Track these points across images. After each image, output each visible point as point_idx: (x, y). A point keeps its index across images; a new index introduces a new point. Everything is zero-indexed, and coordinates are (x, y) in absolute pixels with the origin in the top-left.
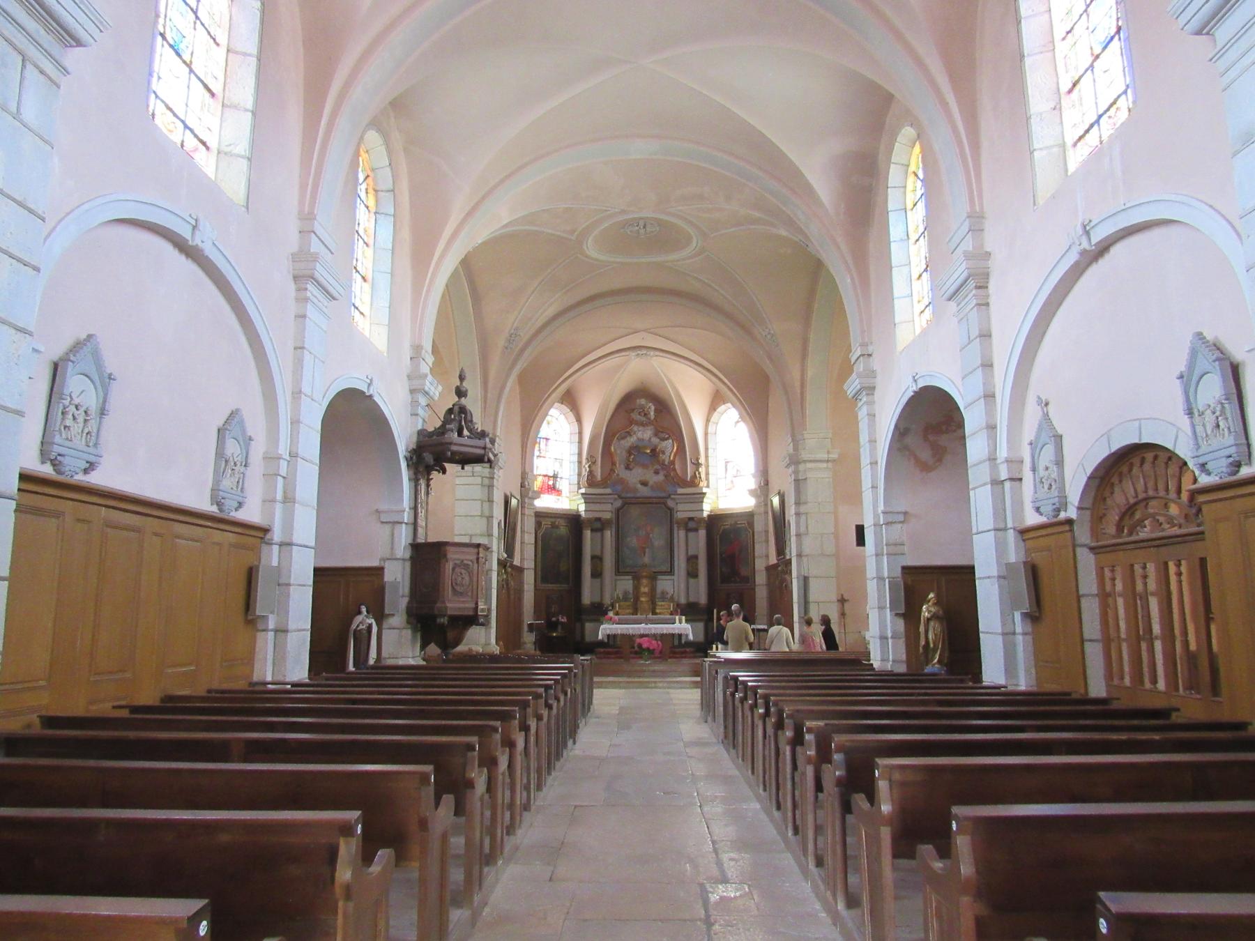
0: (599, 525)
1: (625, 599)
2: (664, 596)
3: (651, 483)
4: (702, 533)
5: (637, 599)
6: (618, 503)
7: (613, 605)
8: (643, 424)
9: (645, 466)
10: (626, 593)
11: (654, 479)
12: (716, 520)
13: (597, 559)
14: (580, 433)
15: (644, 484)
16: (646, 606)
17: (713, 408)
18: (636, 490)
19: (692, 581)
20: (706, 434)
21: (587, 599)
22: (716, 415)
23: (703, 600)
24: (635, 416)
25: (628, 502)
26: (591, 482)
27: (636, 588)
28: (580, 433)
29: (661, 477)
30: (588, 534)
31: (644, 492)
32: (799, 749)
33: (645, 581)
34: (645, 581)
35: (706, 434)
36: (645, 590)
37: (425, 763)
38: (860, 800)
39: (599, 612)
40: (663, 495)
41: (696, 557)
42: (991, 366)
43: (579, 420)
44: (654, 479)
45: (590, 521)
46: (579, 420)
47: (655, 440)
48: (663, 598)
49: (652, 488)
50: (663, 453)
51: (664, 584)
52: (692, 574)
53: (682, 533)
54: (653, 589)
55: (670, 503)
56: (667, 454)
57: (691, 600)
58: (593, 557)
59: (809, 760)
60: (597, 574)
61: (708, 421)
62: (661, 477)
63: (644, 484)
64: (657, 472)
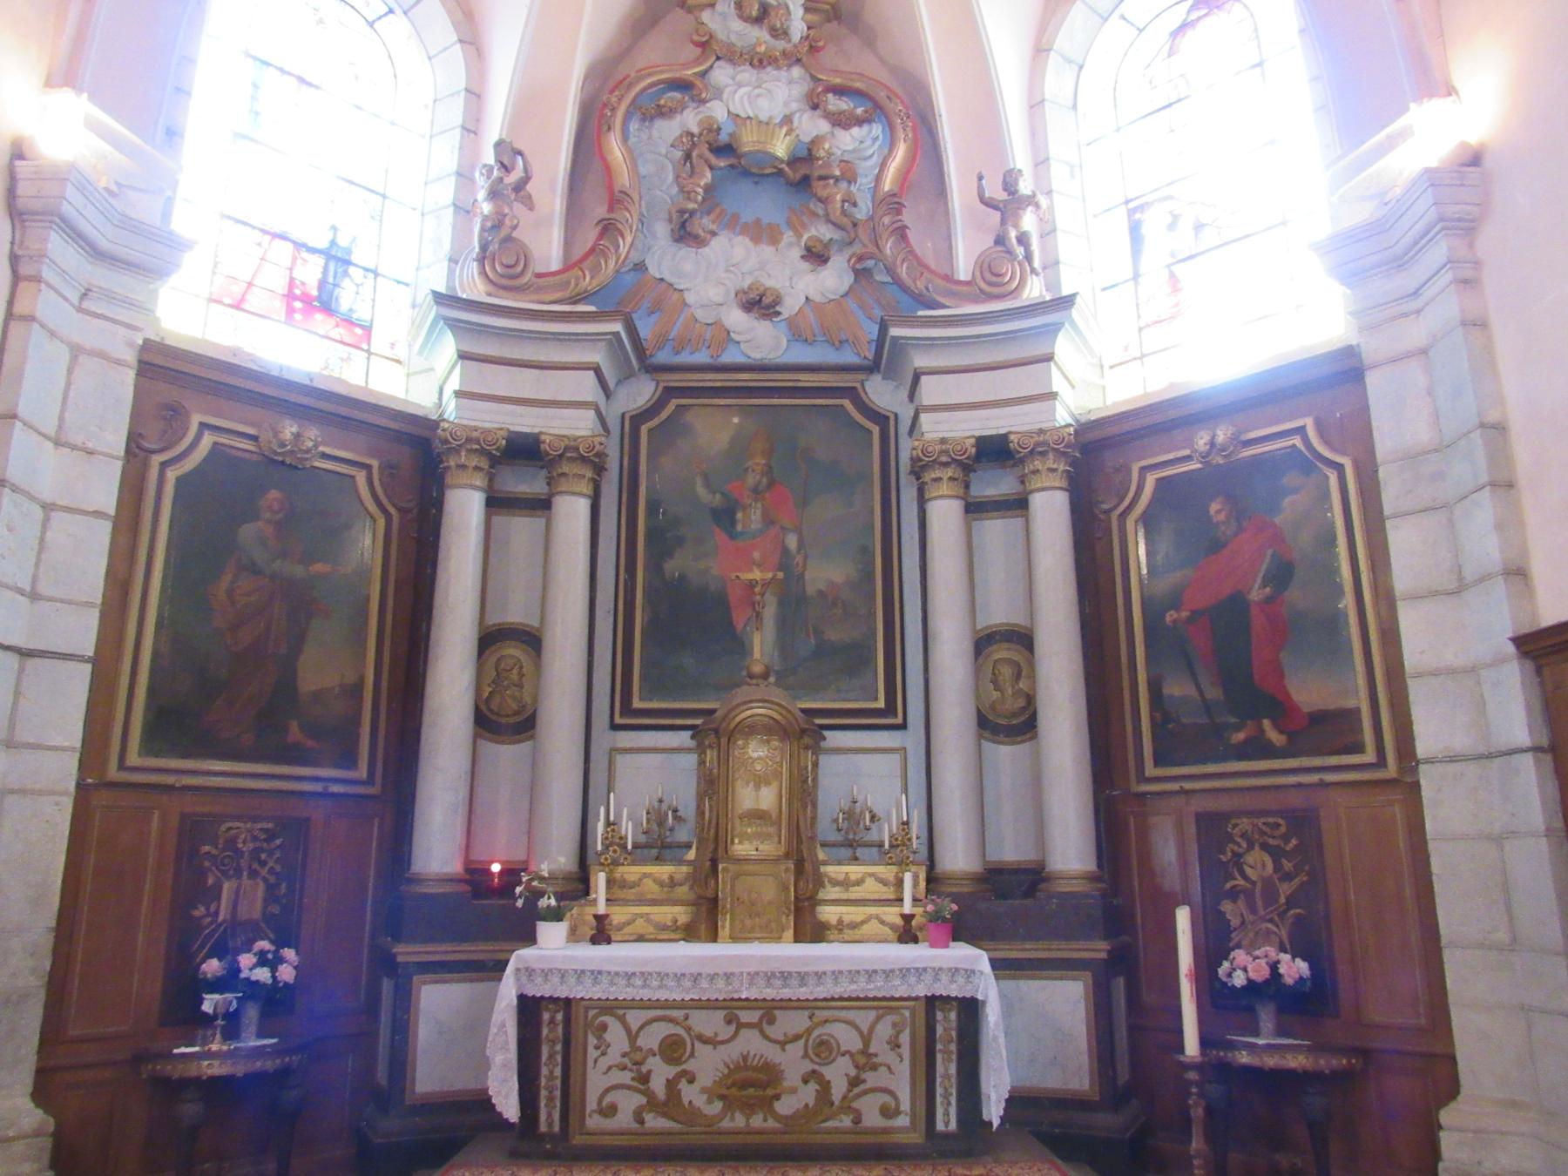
1: (657, 845)
3: (791, 305)
4: (1051, 509)
5: (732, 903)
7: (578, 885)
8: (760, 61)
9: (761, 233)
10: (659, 816)
11: (807, 286)
12: (1095, 458)
13: (507, 644)
14: (475, 95)
15: (760, 304)
16: (768, 888)
18: (725, 337)
19: (1004, 754)
20: (1035, 105)
21: (437, 850)
23: (1071, 851)
25: (678, 387)
26: (501, 253)
27: (713, 786)
28: (475, 95)
29: (833, 279)
30: (465, 508)
31: (761, 341)
35: (1035, 105)
36: (757, 796)
37: (959, 1121)
40: (848, 357)
41: (1023, 639)
42: (1510, 485)
44: (807, 286)
45: (476, 443)
47: (811, 126)
48: (852, 844)
49: (798, 334)
50: (850, 176)
51: (864, 773)
52: (1009, 722)
53: (945, 513)
54: (803, 792)
55: (882, 393)
58: (489, 639)
60: (504, 719)
62: (833, 279)
63: (760, 304)
64: (816, 256)
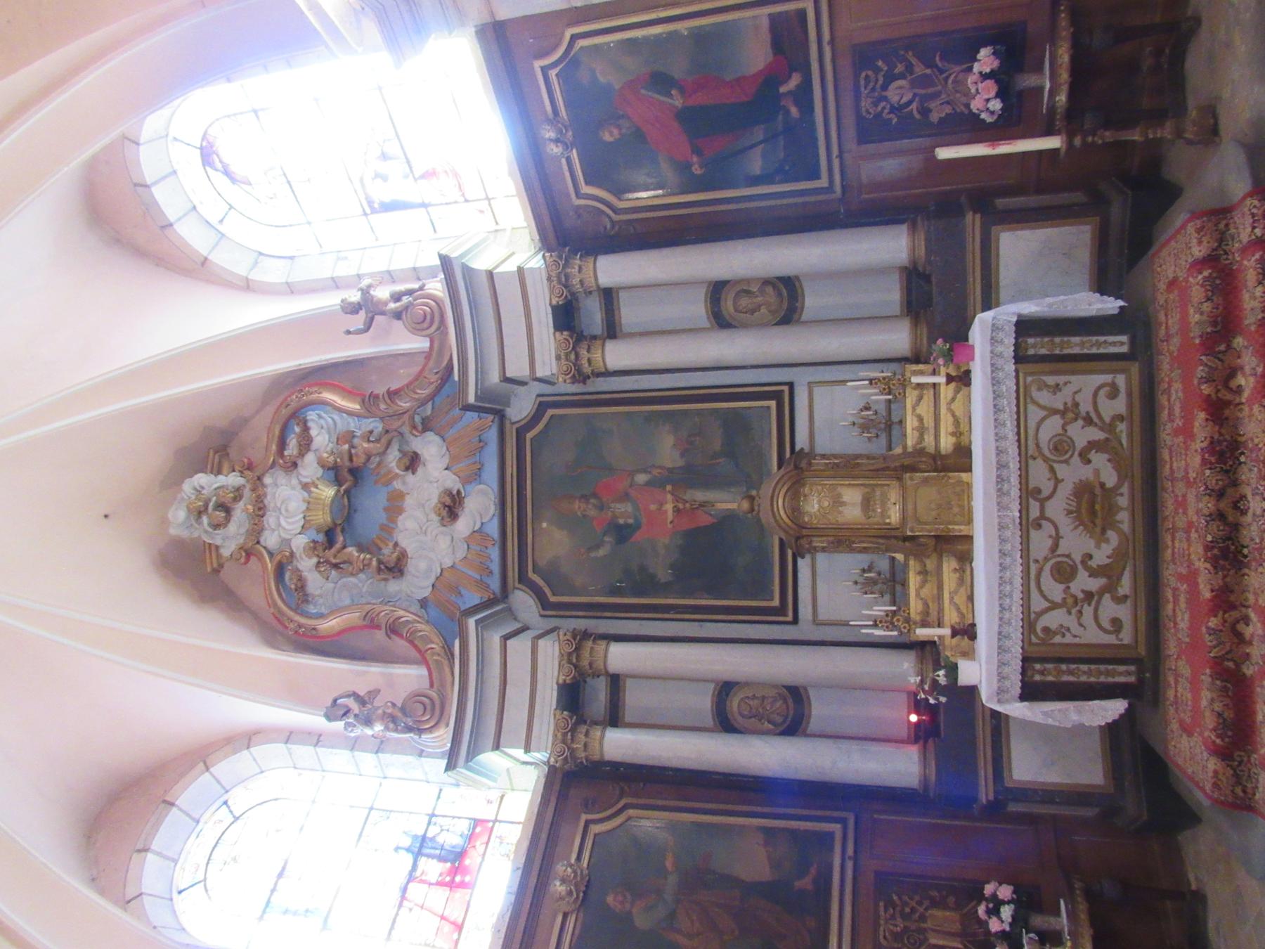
0: (586, 699)
2: (885, 424)
3: (452, 482)
4: (612, 270)
6: (524, 602)
7: (927, 651)
8: (260, 510)
9: (395, 506)
13: (728, 709)
14: (290, 736)
15: (451, 507)
17: (196, 270)
18: (479, 534)
19: (813, 302)
20: (291, 289)
21: (901, 766)
22: (222, 258)
23: (891, 246)
24: (230, 538)
25: (516, 574)
27: (842, 539)
28: (290, 736)
29: (431, 448)
30: (619, 744)
31: (481, 505)
32: (1054, 533)
33: (814, 505)
34: (814, 505)
35: (291, 289)
38: (359, 320)
39: (950, 720)
41: (717, 290)
43: (248, 738)
45: (566, 735)
46: (248, 738)
47: (310, 468)
48: (889, 425)
49: (475, 476)
50: (348, 437)
51: (831, 416)
52: (786, 300)
53: (617, 355)
54: (846, 467)
55: (521, 408)
56: (352, 424)
57: (892, 295)
58: (725, 724)
59: (850, 858)
61: (247, 286)
62: (431, 448)
63: (451, 507)
64: (412, 462)
